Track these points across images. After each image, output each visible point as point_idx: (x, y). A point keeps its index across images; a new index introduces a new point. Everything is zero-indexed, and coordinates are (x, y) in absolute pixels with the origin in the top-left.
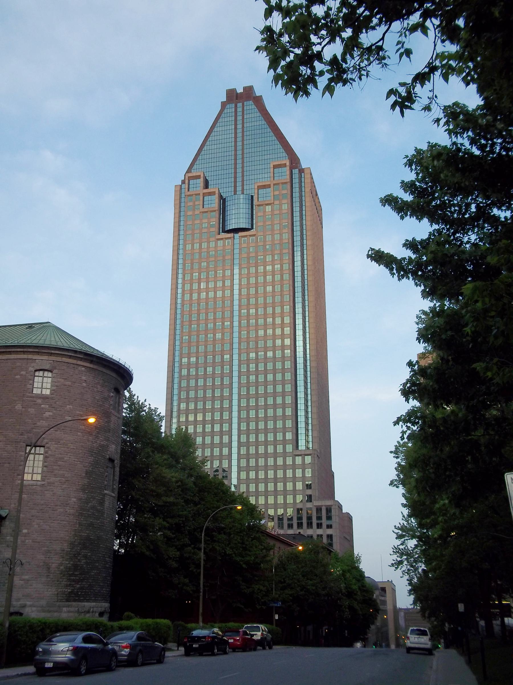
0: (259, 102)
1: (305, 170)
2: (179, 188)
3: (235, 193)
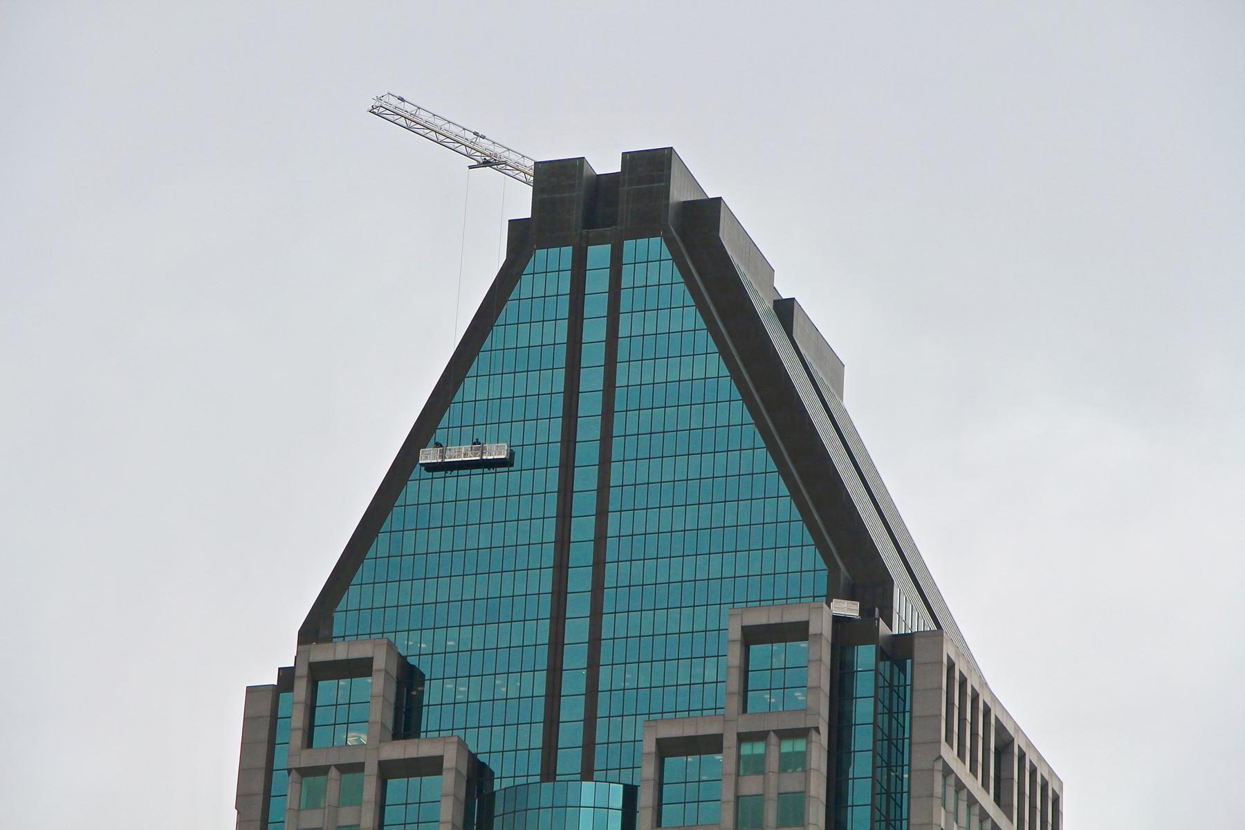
0: (699, 233)
1: (917, 643)
2: (265, 708)
3: (549, 772)
